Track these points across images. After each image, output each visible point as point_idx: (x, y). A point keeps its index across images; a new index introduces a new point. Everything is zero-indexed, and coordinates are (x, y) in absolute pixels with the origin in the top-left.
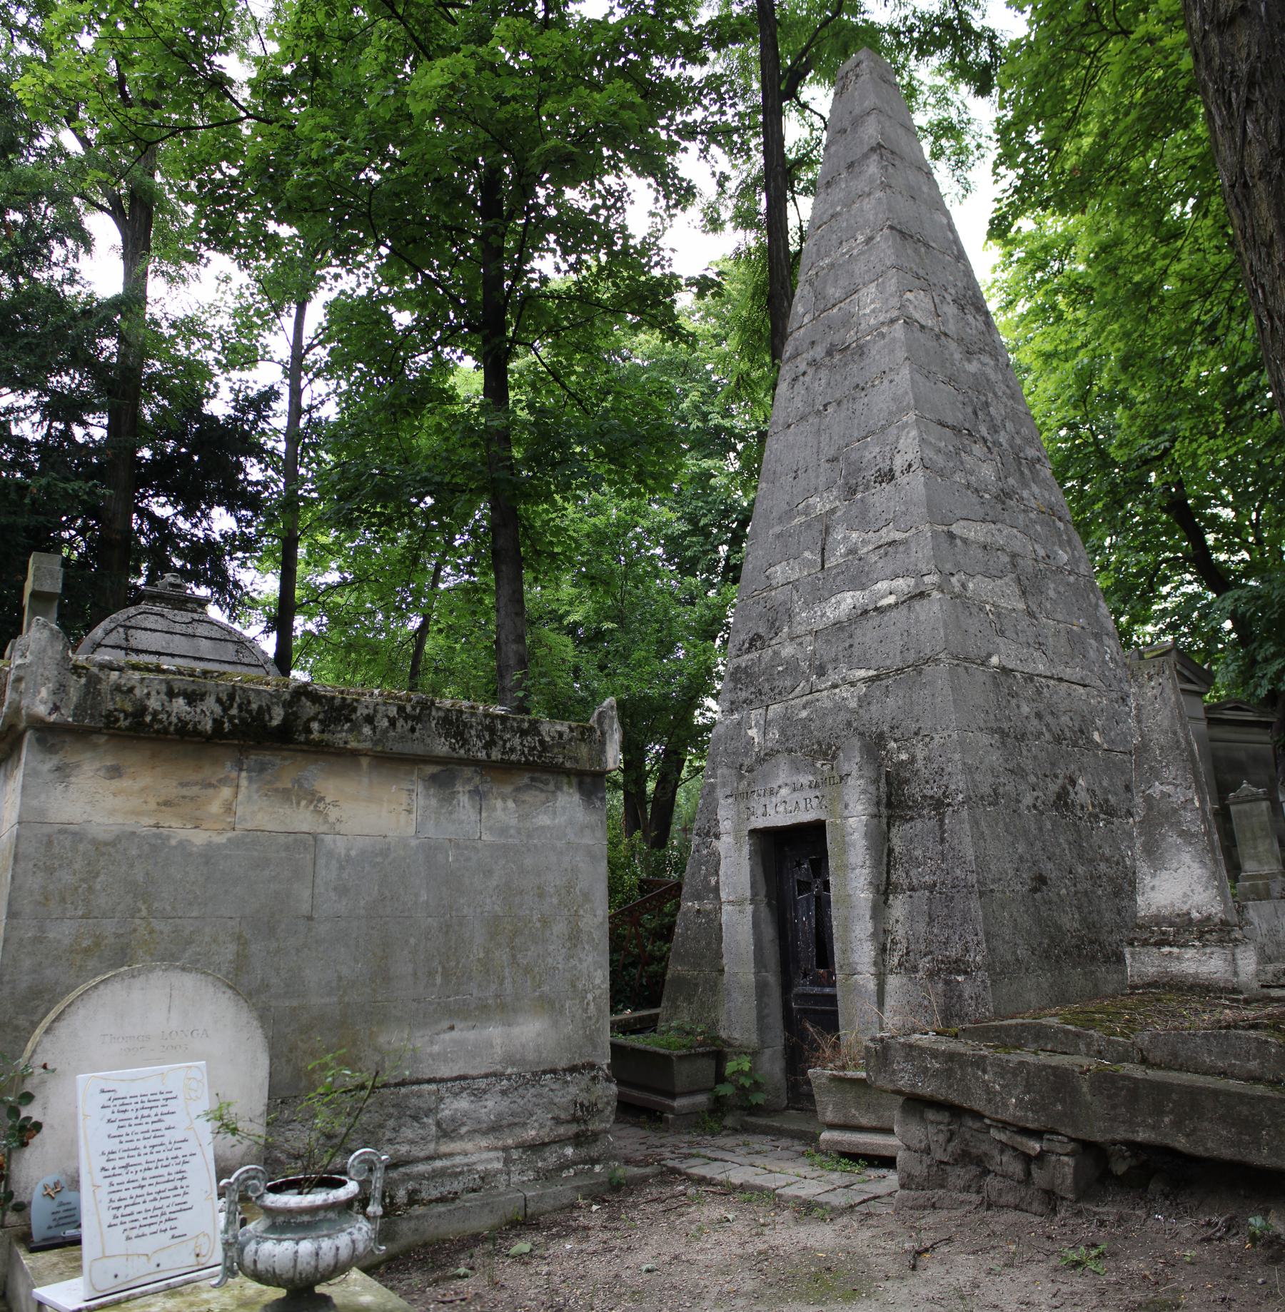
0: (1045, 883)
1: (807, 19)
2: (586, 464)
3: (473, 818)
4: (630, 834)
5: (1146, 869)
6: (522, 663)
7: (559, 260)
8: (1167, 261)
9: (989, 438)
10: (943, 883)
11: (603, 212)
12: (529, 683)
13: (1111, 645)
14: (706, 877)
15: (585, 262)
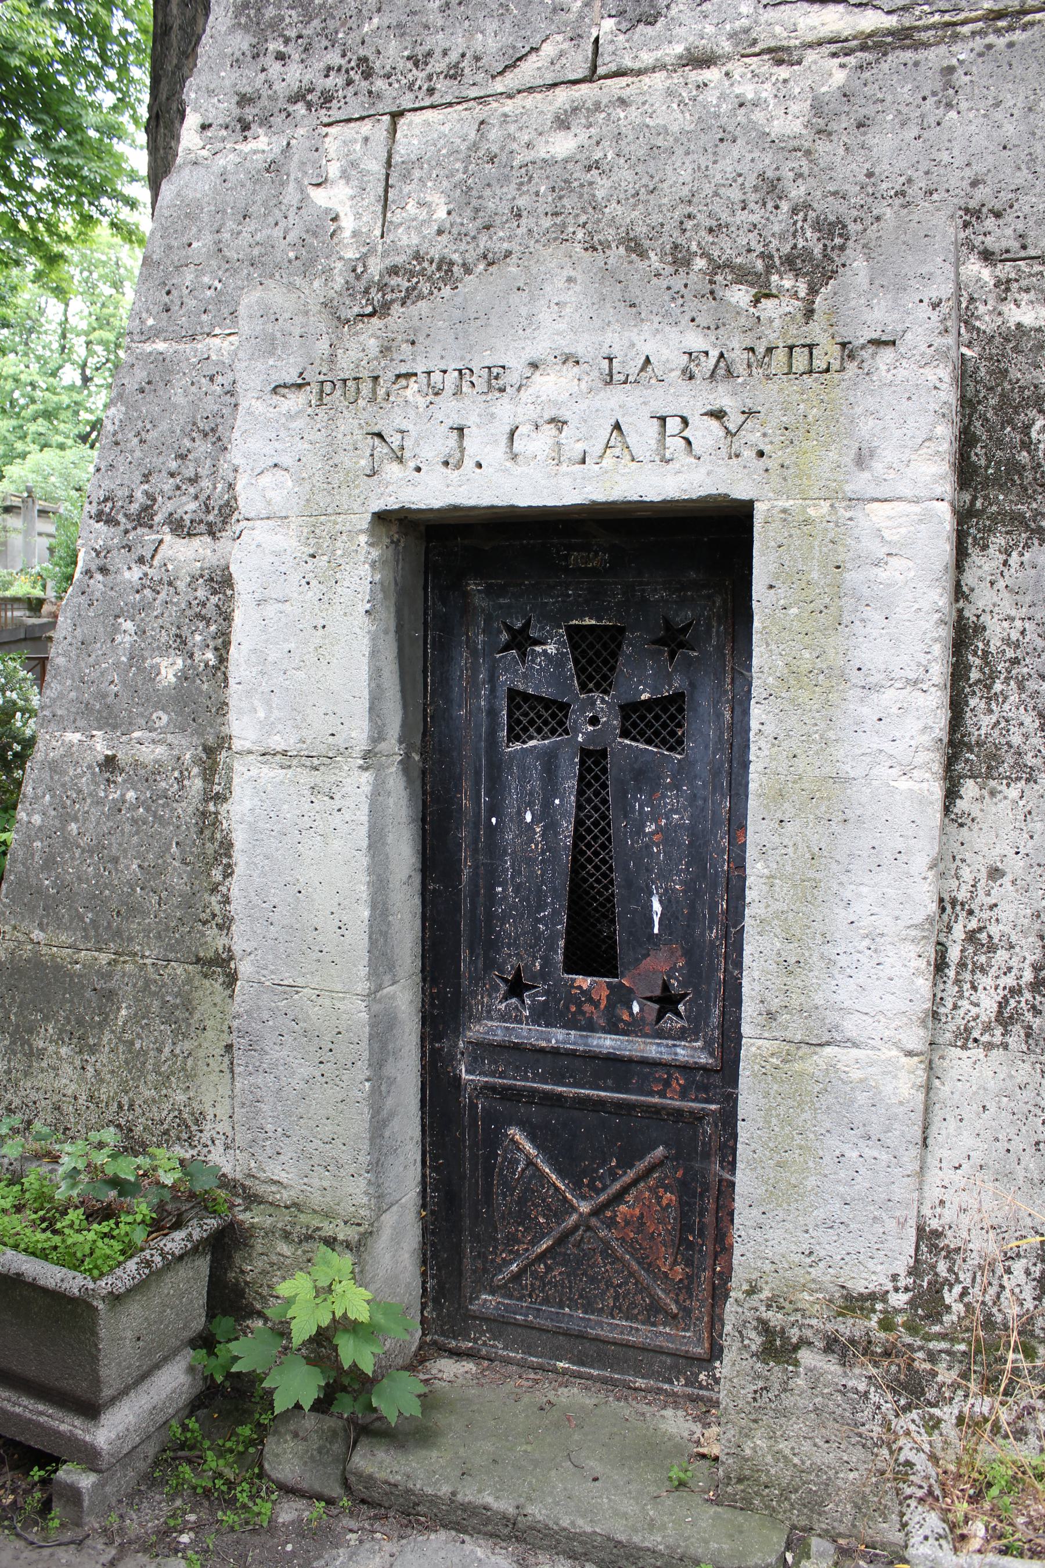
14: (135, 657)
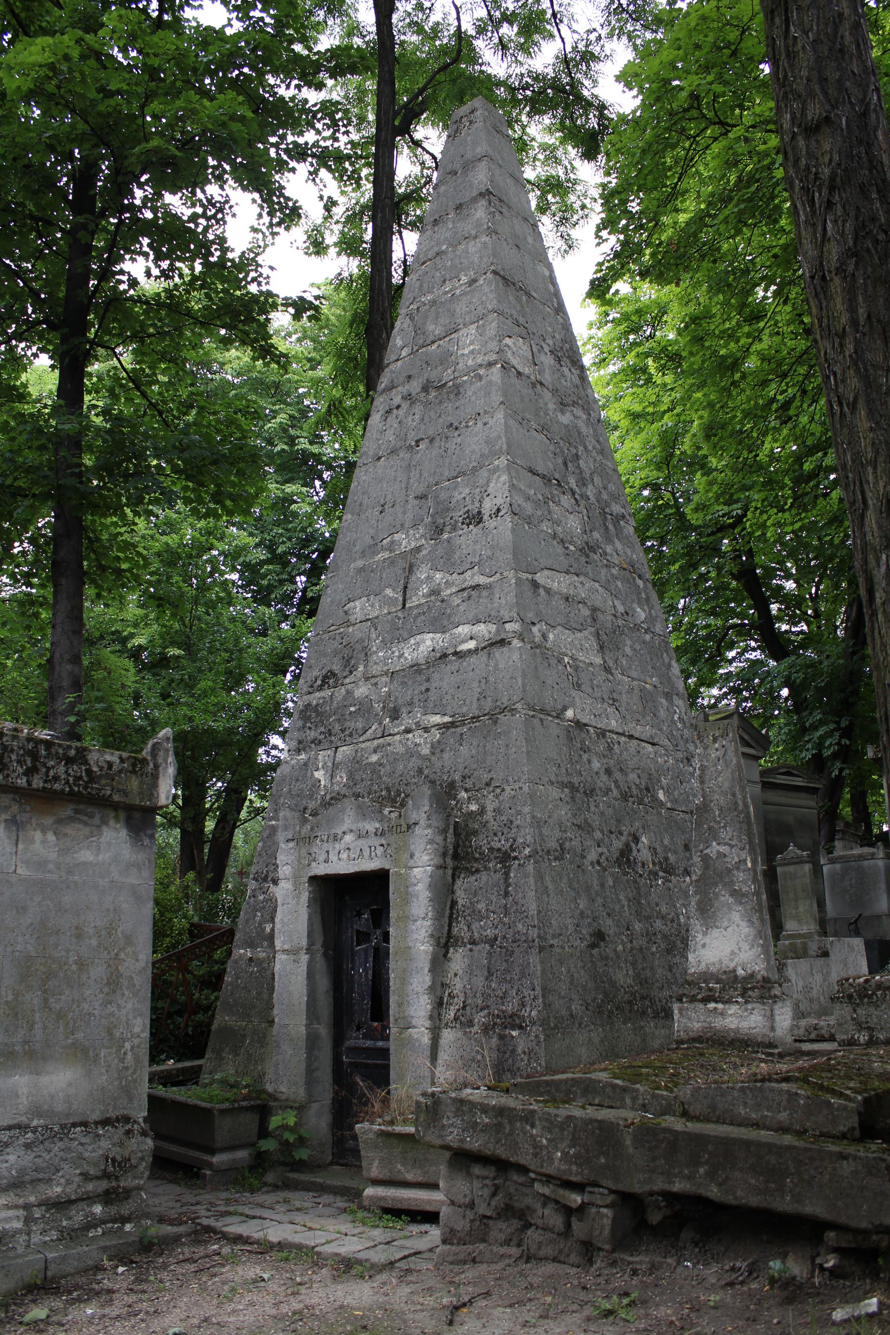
0: (603, 939)
1: (425, 62)
2: (162, 479)
3: (8, 850)
4: (183, 874)
5: (698, 927)
6: (77, 686)
7: (151, 264)
8: (750, 340)
9: (577, 490)
10: (504, 937)
11: (202, 221)
12: (83, 707)
13: (680, 704)
14: (260, 924)
15: (179, 269)
